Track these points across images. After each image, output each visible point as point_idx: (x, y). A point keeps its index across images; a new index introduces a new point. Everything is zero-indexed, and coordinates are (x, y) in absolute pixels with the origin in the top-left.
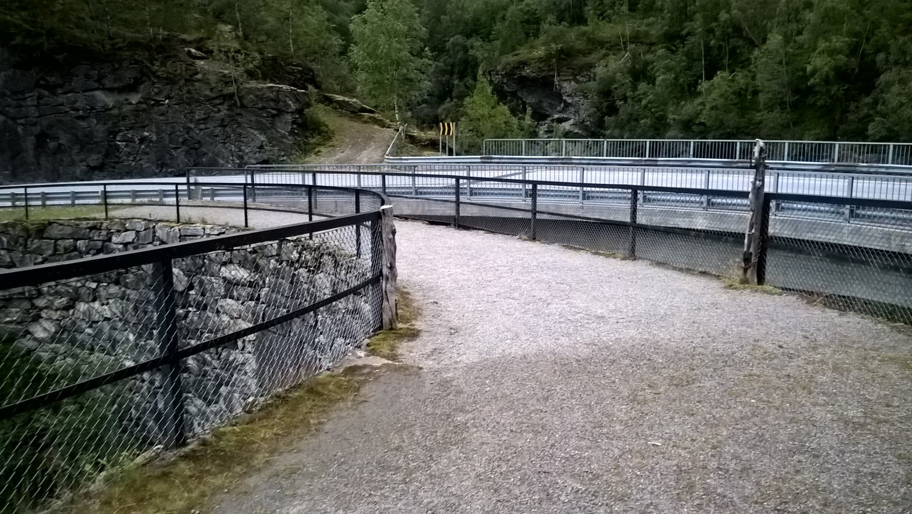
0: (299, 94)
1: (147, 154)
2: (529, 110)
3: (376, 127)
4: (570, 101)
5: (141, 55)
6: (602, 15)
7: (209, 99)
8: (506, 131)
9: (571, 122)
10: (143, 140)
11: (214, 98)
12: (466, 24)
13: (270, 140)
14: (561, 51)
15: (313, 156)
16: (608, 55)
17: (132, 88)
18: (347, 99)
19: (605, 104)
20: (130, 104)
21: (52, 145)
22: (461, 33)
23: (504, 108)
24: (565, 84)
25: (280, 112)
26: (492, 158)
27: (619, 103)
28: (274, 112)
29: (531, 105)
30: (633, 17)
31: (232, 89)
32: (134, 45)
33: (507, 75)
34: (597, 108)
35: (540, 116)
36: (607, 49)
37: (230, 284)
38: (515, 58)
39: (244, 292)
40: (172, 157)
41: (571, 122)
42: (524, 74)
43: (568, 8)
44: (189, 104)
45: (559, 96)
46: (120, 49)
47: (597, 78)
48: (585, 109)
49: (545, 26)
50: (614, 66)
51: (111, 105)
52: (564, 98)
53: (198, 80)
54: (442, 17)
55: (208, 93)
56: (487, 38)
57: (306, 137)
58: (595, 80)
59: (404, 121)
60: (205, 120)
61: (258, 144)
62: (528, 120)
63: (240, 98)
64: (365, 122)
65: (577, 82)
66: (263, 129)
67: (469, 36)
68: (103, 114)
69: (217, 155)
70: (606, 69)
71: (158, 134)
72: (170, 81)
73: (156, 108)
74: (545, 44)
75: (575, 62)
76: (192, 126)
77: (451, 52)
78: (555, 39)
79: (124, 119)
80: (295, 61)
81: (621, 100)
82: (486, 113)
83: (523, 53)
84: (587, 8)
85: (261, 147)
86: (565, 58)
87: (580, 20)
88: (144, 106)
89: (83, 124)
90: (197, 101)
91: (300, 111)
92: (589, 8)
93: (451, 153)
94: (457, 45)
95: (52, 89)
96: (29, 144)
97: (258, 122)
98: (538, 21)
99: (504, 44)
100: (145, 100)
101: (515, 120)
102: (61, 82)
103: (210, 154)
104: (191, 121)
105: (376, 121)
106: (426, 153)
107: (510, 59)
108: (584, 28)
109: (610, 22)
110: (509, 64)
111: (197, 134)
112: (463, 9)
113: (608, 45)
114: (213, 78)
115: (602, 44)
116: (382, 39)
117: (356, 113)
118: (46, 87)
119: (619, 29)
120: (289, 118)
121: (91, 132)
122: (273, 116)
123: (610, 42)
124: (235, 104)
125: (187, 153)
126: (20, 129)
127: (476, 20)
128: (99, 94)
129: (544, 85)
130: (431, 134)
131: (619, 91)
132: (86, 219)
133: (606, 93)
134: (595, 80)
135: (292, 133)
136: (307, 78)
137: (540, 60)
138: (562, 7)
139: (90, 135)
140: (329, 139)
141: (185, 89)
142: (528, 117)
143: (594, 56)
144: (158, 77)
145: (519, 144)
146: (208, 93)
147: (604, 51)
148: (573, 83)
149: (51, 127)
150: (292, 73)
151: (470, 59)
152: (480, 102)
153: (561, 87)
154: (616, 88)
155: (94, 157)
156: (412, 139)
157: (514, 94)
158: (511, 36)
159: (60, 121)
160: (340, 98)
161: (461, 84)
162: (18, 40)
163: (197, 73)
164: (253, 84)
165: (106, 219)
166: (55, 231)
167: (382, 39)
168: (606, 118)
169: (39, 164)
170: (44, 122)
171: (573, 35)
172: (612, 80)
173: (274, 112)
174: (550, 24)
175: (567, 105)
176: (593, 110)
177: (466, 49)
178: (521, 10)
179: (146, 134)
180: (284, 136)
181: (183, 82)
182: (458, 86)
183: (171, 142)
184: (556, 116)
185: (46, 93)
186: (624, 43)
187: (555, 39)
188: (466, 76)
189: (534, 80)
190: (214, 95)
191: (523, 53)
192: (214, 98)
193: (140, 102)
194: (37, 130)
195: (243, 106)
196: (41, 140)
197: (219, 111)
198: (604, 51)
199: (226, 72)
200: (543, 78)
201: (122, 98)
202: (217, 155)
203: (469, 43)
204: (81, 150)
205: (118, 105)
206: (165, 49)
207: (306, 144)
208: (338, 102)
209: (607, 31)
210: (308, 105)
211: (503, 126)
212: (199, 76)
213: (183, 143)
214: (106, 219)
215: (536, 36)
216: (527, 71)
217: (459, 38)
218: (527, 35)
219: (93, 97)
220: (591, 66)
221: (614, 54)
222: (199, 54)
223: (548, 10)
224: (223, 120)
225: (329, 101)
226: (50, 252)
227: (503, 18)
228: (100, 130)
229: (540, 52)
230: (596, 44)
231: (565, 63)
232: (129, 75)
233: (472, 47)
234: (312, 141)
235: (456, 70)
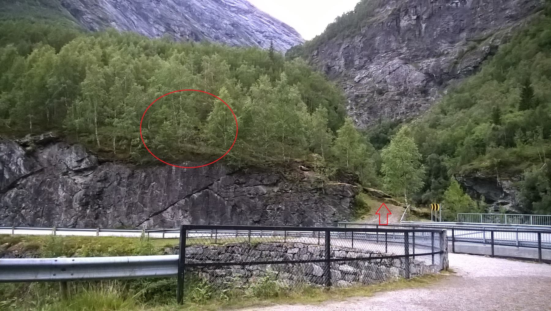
0: (354, 188)
1: (280, 216)
2: (483, 198)
3: (393, 205)
4: (508, 192)
5: (280, 169)
6: (525, 142)
7: (310, 190)
8: (470, 209)
9: (510, 205)
10: (278, 209)
11: (313, 190)
12: (438, 147)
13: (339, 210)
14: (500, 163)
15: (361, 220)
16: (532, 165)
17: (275, 185)
18: (376, 190)
19: (532, 195)
20: (274, 192)
21: (238, 210)
22: (435, 152)
23: (467, 196)
24: (504, 182)
25: (344, 197)
26: (463, 224)
27: (541, 194)
28: (341, 197)
29: (484, 195)
30: (546, 142)
31: (322, 185)
32: (278, 164)
33: (466, 176)
34: (527, 197)
35: (489, 201)
36: (531, 161)
37: (344, 274)
38: (471, 166)
39: (351, 277)
40: (292, 218)
41: (510, 205)
42: (477, 176)
43: (503, 138)
44: (300, 192)
45: (501, 189)
46: (272, 166)
47: (525, 178)
48: (519, 197)
49: (489, 149)
50: (536, 172)
51: (265, 192)
52: (504, 190)
53: (305, 181)
54: (424, 143)
55: (310, 187)
56: (452, 155)
57: (357, 210)
58: (524, 180)
59: (410, 203)
60: (307, 200)
61: (333, 212)
62: (482, 203)
63: (325, 190)
64: (387, 203)
65: (512, 181)
66: (335, 205)
67: (440, 154)
68: (261, 196)
69: (312, 218)
70: (531, 173)
71: (285, 206)
72: (292, 181)
73: (285, 194)
74: (489, 158)
75: (510, 169)
76: (301, 203)
77: (429, 163)
78: (496, 156)
79: (271, 199)
80: (349, 171)
81: (543, 192)
82: (458, 199)
83: (476, 164)
84: (515, 138)
85: (334, 214)
86: (503, 166)
87: (513, 145)
88: (280, 193)
89: (253, 201)
90: (305, 191)
91: (353, 197)
92: (517, 137)
93: (438, 221)
94: (434, 159)
95: (240, 184)
96: (229, 209)
97: (333, 201)
98: (484, 146)
99: (463, 158)
100: (281, 190)
101: (475, 203)
102: (244, 182)
103: (309, 217)
104: (301, 201)
105: (392, 202)
106: (422, 220)
107: (467, 167)
108: (514, 149)
109: (532, 146)
110: (466, 170)
111: (303, 207)
112: (436, 139)
113: (531, 159)
114: (313, 180)
115: (527, 158)
116: (398, 161)
117: (381, 198)
118: (239, 184)
119: (537, 150)
120: (348, 200)
121: (256, 205)
122: (341, 199)
123: (533, 157)
124: (322, 193)
125: (298, 216)
126: (226, 203)
127: (444, 145)
128: (260, 187)
129: (490, 182)
130: (425, 210)
131: (541, 186)
132: (275, 242)
133: (532, 188)
134: (524, 180)
135: (350, 208)
136: (355, 180)
137: (487, 168)
138: (500, 137)
139: (255, 207)
140: (368, 211)
141: (299, 186)
142: (482, 202)
143: (521, 167)
144: (287, 179)
145: (479, 217)
146: (310, 187)
147: (529, 163)
148: (509, 181)
149: (239, 202)
150: (348, 177)
151: (442, 167)
152: (453, 193)
153: (502, 184)
154: (539, 185)
155: (256, 216)
156: (415, 213)
157: (471, 188)
158: (467, 154)
159: (243, 199)
160: (372, 190)
161: (436, 181)
162: (231, 163)
163: (305, 178)
164: (331, 183)
165: (285, 242)
166: (261, 247)
167: (398, 161)
168: (533, 203)
169: (232, 219)
170: (236, 199)
171: (507, 154)
172: (535, 180)
173: (341, 197)
174: (492, 147)
175: (507, 195)
176: (523, 198)
177: (439, 162)
178: (473, 139)
179: (280, 206)
180: (345, 209)
181: (298, 182)
182: (434, 182)
183: (291, 211)
184: (499, 201)
185: (238, 186)
186: (542, 158)
187: (496, 156)
188: (439, 177)
189: (483, 180)
190: (312, 188)
191: (476, 164)
192: (313, 190)
193: (278, 191)
194: (232, 203)
195: (326, 194)
196: (234, 207)
197: (314, 196)
198: (529, 163)
199: (319, 177)
200: (490, 178)
201: (270, 189)
202: (312, 218)
203: (441, 158)
204: (251, 213)
205: (268, 192)
206: (289, 166)
207: (357, 213)
208: (371, 192)
209: (529, 151)
210: (357, 194)
211: (468, 206)
212: (306, 179)
213: (297, 211)
214: (285, 242)
215: (484, 153)
216: (479, 174)
217: (434, 155)
218: (478, 153)
219: (258, 188)
220: (521, 171)
221: (536, 165)
222: (305, 168)
223: (490, 139)
224: (316, 200)
225: (366, 191)
226: (258, 256)
227: (462, 144)
228: (260, 204)
229: (487, 163)
230: (523, 158)
231: (503, 169)
232: (274, 178)
233: (443, 160)
234: (359, 211)
235: (433, 173)
